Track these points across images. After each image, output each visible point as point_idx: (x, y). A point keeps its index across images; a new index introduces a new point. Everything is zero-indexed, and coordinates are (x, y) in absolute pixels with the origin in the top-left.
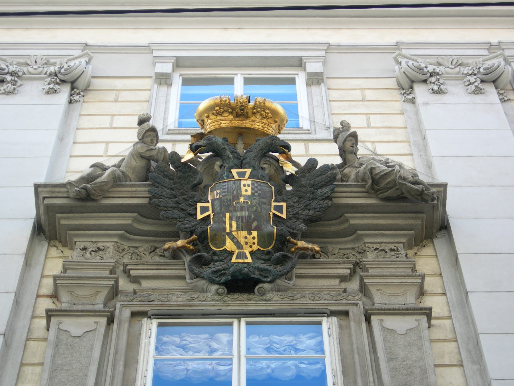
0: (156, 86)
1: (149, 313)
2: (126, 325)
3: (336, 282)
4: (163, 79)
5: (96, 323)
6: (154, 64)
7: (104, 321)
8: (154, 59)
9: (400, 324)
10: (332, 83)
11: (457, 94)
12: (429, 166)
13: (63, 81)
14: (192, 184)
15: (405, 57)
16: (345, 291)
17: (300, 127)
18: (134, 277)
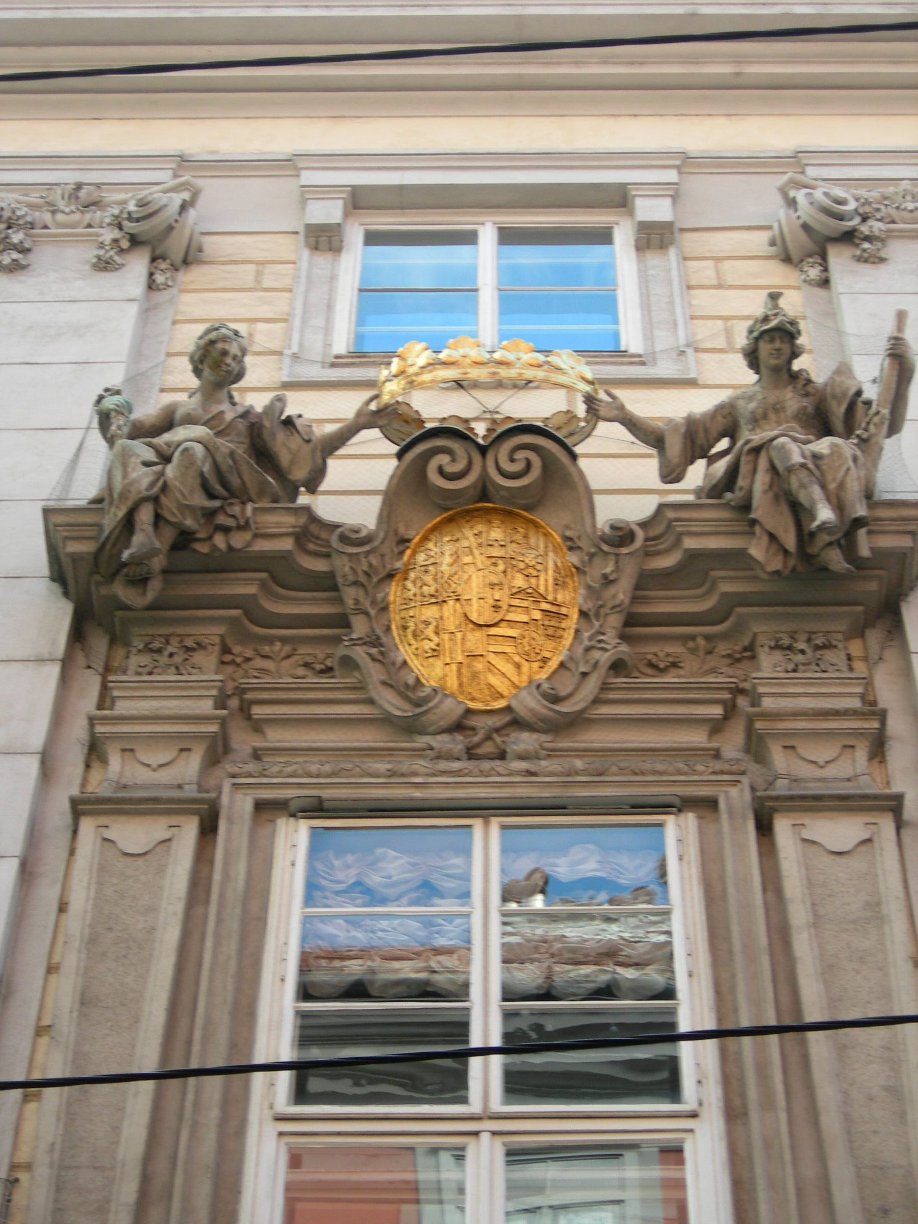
0: (306, 253)
1: (293, 805)
6: (303, 202)
8: (303, 193)
9: (840, 831)
13: (135, 241)
14: (76, 944)
17: (623, 349)
18: (258, 720)
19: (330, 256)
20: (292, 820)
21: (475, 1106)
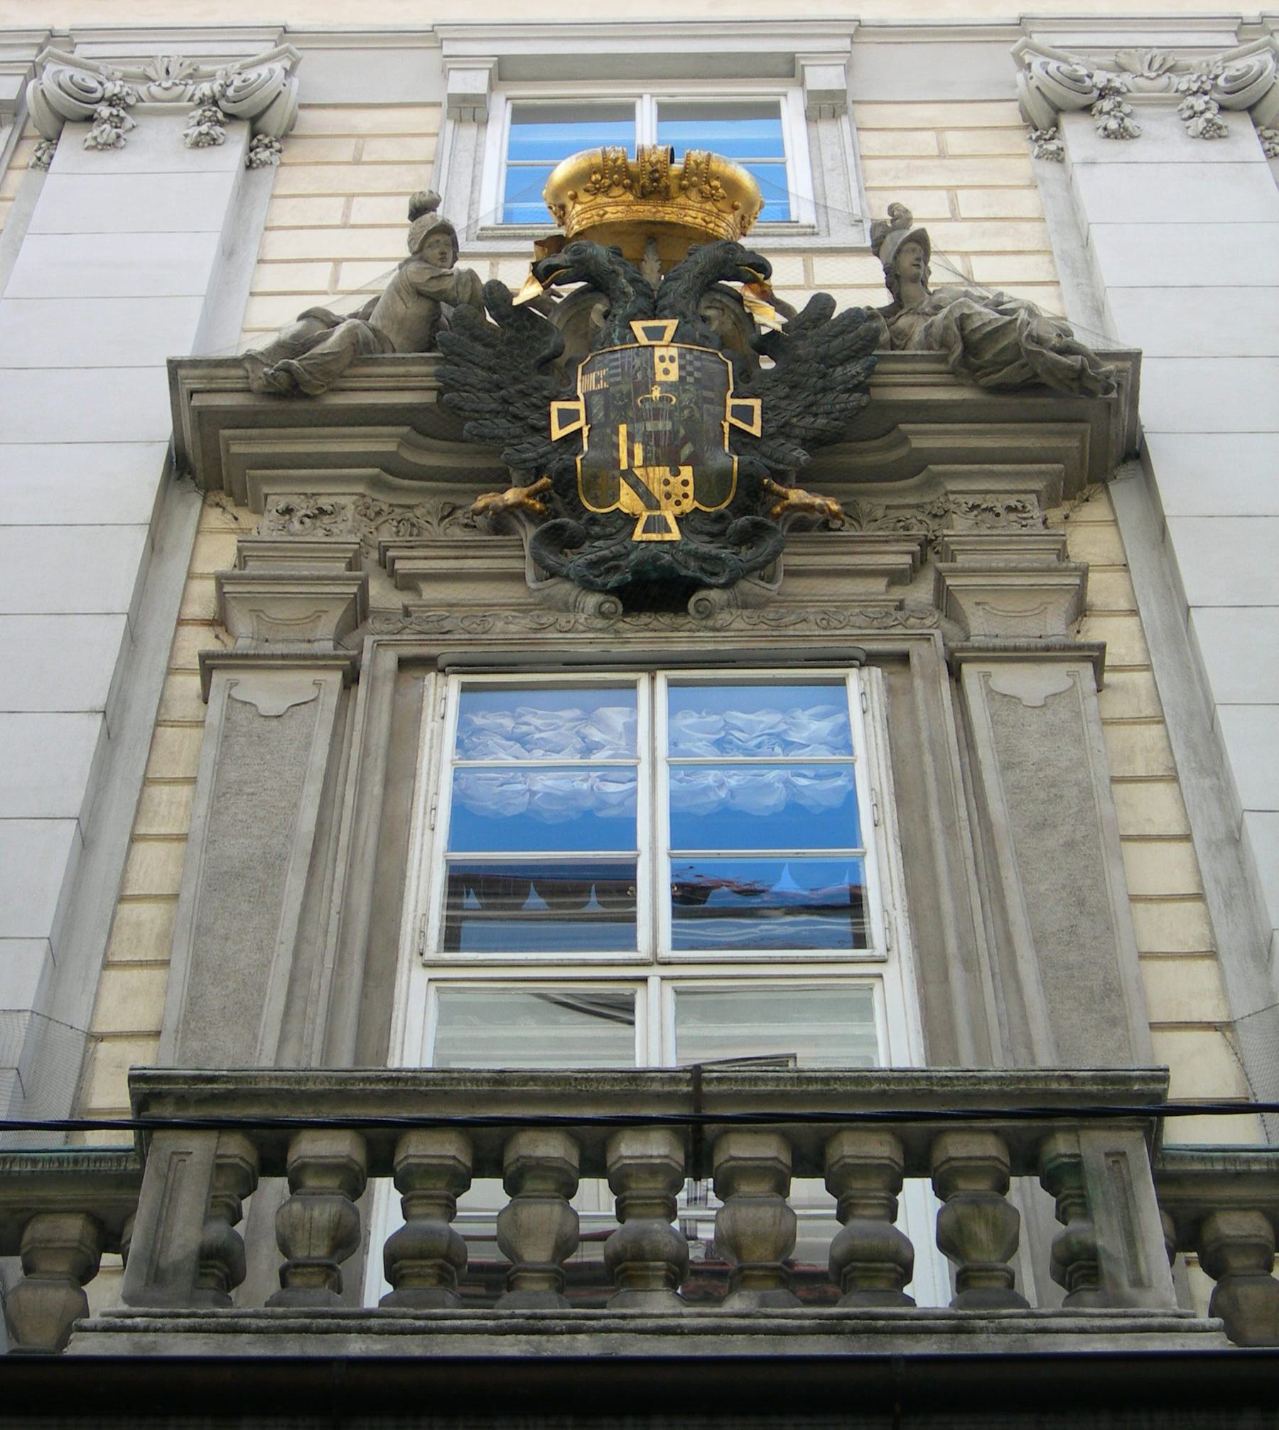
0: (450, 125)
2: (386, 690)
3: (879, 585)
4: (468, 110)
5: (317, 684)
6: (445, 73)
7: (335, 678)
10: (868, 115)
11: (1163, 138)
12: (1098, 310)
15: (1039, 51)
16: (900, 606)
19: (43, 172)
20: (440, 676)
21: (643, 949)
